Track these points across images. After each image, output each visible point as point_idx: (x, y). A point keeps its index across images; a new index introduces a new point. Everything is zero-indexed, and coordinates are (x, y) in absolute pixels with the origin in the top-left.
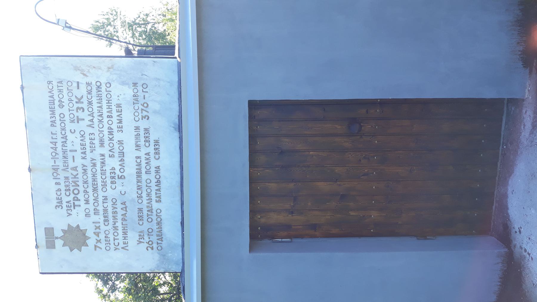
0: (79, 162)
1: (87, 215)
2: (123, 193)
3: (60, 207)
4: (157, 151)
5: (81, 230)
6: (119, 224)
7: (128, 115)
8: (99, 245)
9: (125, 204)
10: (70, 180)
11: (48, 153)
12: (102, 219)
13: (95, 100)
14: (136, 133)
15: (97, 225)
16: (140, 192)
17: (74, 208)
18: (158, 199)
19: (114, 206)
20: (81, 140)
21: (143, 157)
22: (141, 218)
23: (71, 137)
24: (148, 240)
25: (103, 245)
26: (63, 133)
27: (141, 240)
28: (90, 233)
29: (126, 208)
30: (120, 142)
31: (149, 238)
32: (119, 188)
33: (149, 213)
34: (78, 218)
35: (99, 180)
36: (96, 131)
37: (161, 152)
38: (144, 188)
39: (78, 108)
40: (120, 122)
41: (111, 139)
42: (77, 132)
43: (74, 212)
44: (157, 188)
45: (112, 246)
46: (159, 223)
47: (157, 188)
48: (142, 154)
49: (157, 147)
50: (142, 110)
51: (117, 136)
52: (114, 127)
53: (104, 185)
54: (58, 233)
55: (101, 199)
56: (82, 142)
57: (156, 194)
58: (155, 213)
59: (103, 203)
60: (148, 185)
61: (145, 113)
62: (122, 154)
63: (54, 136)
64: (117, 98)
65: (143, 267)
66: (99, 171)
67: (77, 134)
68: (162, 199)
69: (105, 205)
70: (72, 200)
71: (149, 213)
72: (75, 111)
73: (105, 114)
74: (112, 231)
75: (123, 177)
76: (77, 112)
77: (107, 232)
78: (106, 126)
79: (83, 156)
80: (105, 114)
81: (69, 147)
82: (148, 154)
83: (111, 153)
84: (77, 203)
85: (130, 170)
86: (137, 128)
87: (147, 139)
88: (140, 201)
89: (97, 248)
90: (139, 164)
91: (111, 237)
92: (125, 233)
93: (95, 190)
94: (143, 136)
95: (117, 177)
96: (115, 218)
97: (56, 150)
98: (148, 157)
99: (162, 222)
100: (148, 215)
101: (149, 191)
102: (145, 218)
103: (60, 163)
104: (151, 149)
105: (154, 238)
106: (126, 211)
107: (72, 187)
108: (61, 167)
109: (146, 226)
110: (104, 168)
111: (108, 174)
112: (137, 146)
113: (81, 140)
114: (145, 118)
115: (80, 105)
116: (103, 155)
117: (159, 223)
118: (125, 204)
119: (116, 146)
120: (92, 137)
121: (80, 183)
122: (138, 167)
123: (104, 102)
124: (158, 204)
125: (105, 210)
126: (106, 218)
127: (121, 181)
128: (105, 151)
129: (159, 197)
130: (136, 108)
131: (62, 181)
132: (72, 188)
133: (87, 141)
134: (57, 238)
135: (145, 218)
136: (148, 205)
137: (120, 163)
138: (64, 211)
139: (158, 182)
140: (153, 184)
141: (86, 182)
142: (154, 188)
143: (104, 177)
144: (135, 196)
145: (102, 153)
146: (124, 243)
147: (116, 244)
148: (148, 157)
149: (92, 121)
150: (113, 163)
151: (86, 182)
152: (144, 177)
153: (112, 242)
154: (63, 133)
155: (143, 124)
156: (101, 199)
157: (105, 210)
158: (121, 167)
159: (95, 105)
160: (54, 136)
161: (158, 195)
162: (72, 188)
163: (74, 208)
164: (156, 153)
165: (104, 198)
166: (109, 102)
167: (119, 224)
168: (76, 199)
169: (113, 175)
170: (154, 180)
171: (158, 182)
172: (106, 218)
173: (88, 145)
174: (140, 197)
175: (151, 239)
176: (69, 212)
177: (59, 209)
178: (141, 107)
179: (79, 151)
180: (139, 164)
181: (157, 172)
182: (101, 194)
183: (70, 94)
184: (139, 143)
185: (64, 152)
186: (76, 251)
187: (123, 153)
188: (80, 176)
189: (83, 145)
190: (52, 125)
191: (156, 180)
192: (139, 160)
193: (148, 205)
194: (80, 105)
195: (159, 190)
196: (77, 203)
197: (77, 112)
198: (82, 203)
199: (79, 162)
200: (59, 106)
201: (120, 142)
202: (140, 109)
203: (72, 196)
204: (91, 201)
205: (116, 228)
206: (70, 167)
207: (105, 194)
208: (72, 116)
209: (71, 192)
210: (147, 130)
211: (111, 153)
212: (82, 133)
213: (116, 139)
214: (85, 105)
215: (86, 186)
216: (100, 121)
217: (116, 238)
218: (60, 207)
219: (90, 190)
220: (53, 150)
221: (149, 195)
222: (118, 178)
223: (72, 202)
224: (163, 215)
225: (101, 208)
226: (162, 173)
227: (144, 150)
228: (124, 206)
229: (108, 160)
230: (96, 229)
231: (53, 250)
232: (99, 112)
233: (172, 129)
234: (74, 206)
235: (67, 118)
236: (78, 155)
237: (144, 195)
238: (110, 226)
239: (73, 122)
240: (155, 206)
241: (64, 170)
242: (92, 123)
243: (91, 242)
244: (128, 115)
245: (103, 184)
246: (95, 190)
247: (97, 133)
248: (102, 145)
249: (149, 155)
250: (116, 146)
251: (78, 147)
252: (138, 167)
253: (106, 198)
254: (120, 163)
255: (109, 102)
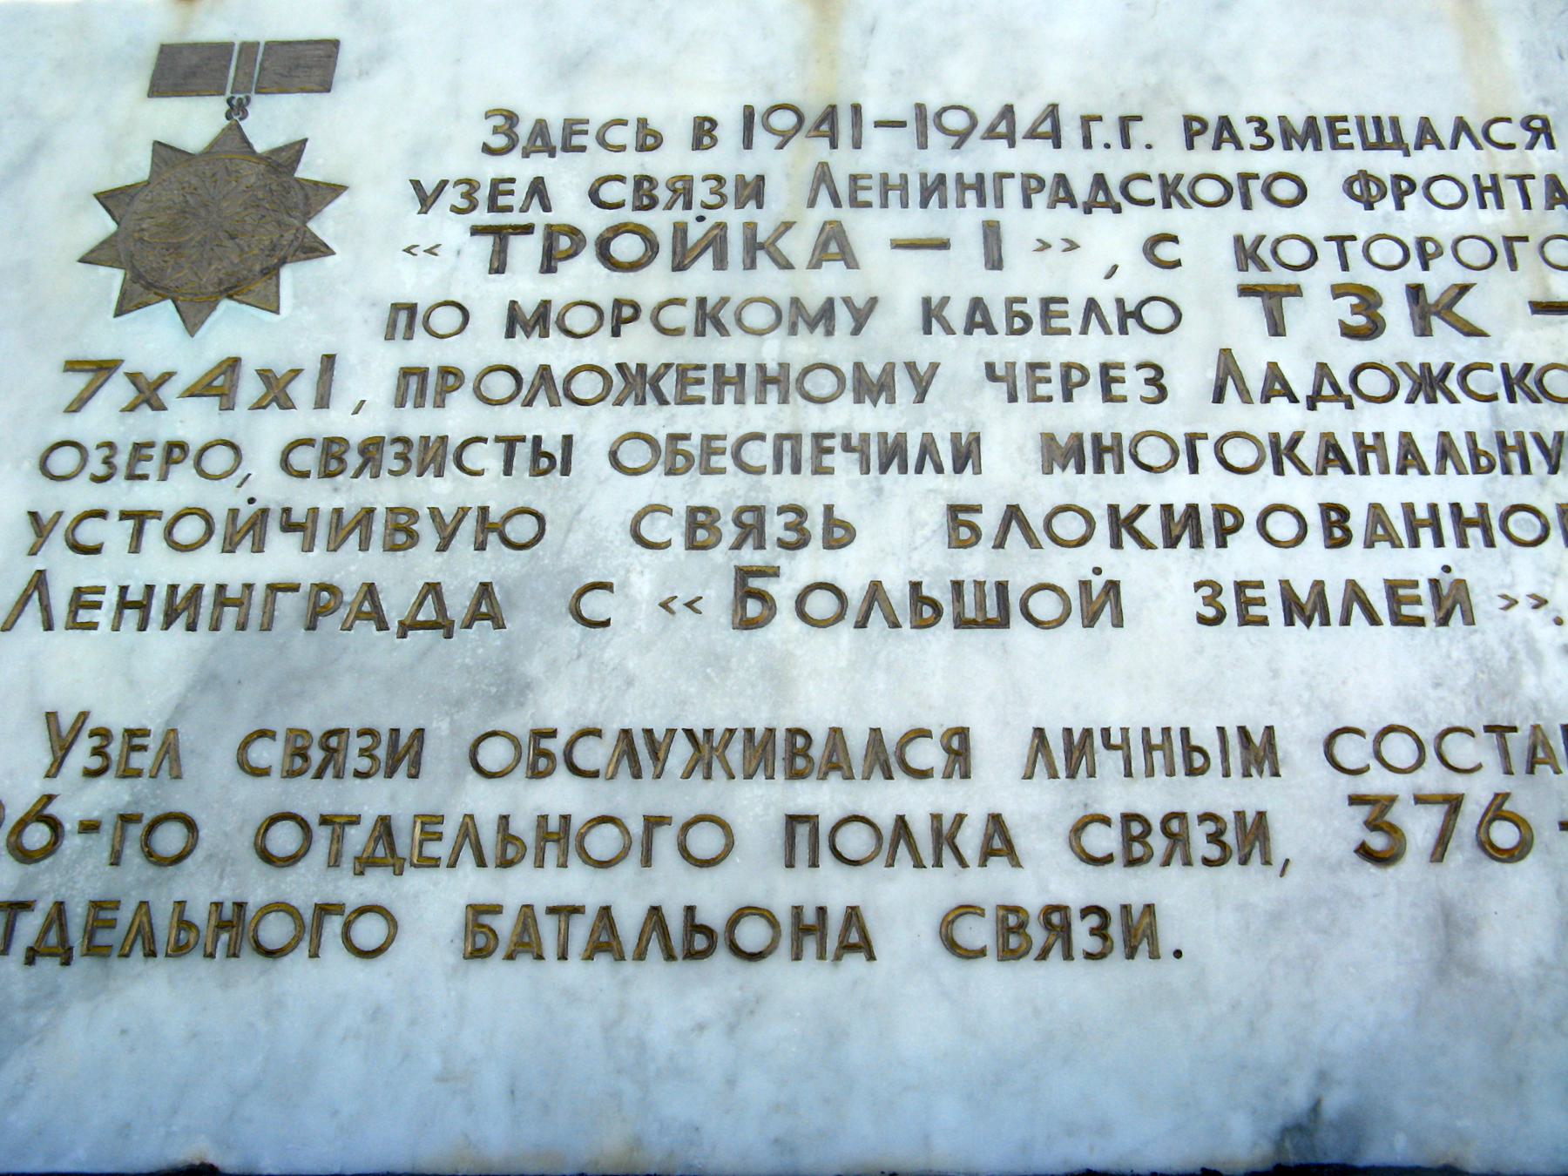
0: (901, 282)
1: (405, 318)
2: (594, 605)
3: (499, 141)
4: (1037, 933)
5: (272, 273)
6: (282, 558)
7: (1377, 673)
8: (118, 390)
9: (474, 617)
10: (734, 218)
11: (966, 82)
12: (356, 429)
13: (1463, 418)
14: (1204, 737)
15: (302, 390)
16: (592, 754)
17: (476, 231)
18: (504, 925)
19: (469, 525)
20: (1092, 306)
21: (969, 801)
22: (316, 753)
23: (1114, 238)
24: (69, 811)
25: (105, 419)
26: (1139, 190)
27: (84, 745)
28: (233, 330)
29: (443, 625)
30: (1102, 602)
31: (89, 827)
32: (643, 577)
33: (357, 838)
34: (379, 256)
35: (727, 419)
36: (1189, 407)
37: (1027, 972)
38: (632, 799)
39: (1368, 301)
40: (1304, 608)
41: (1123, 525)
42: (1160, 282)
43: (448, 228)
44: (629, 923)
45: (79, 496)
46: (235, 930)
47: (629, 923)
48: (999, 786)
49: (1081, 933)
50: (1454, 803)
51: (1161, 581)
52: (1245, 557)
53: (673, 455)
54: (272, 121)
55: (545, 422)
56: (1076, 309)
57: (565, 912)
58: (353, 890)
59: (510, 443)
60: (665, 841)
61: (1420, 827)
62: (991, 610)
63: (1104, 132)
64: (1521, 592)
65: (1107, 146)
66: (813, 419)
67: (1138, 280)
68: (501, 978)
69: (487, 458)
70: (553, 218)
71: (357, 838)
72: (1342, 278)
73: (1356, 493)
74: (220, 499)
75: (753, 608)
76: (1338, 291)
77: (218, 460)
78: (1250, 495)
79: (956, 314)
80: (1356, 493)
81: (1024, 224)
82: (1000, 841)
83: (989, 521)
84: (525, 250)
85: (827, 680)
86: (1259, 752)
87: (1158, 842)
88: (495, 754)
89: (79, 381)
90: (886, 758)
91: (181, 489)
92: (183, 607)
93: (638, 383)
94: (1192, 810)
95: (750, 556)
96: (352, 527)
97: (991, 134)
98: (970, 839)
99: (250, 962)
100: (337, 823)
101: (603, 842)
102: (313, 797)
103: (881, 153)
104: (1047, 878)
105: (79, 875)
106: (405, 629)
107: (675, 214)
108: (844, 162)
109: (224, 799)
110: (839, 460)
111: (780, 489)
112: (1079, 749)
113: (1092, 306)
114: (1373, 825)
115: (1396, 311)
116: (967, 454)
117: (235, 930)
118: (474, 617)
119: (1065, 568)
120: (1134, 384)
121: (701, 279)
122: (857, 743)
123: (1467, 490)
124: (453, 920)
125: (432, 455)
126: (353, 459)
127: (719, 595)
128: (1009, 473)
129: (526, 944)
130: (1461, 750)
131: (726, 158)
132: (660, 221)
133: (1091, 349)
134: (237, 109)
135: (313, 797)
136: (450, 829)
137: (898, 593)
138: (463, 159)
139: (695, 940)
140: (674, 886)
141: (708, 317)
142: (628, 895)
143: (758, 454)
144: (558, 708)
145: (990, 453)
146: (81, 599)
147: (89, 533)
148: (970, 839)
149: (1276, 385)
150: (896, 536)
151: (708, 317)
152: (756, 804)
153: (122, 495)
154: (1139, 190)
155: (1307, 809)
156: (545, 422)
157: (432, 455)
158: (856, 597)
159: (1425, 422)
160: (1104, 132)
161: (548, 928)
162: (660, 221)
163: (476, 231)
164: (1011, 922)
165: (552, 445)
166: (1472, 524)
167: (282, 558)
168: (564, 243)
169: (775, 527)
170: (713, 896)
171: (695, 940)
172: (353, 459)
173: (1058, 351)
174: (540, 755)
175: (73, 842)
176: (452, 196)
177: (483, 132)
178: (1477, 793)
179: (995, 289)
180: (886, 758)
181: (802, 930)
182: (596, 428)
183: (1474, 252)
184: (1110, 762)
185: (980, 188)
186: (101, 225)
187: (1003, 622)
188: (768, 280)
189: (1046, 315)
190: (1193, 128)
191: (714, 914)
192: (927, 754)
193: (450, 829)
194: (1396, 311)
195: (604, 939)
196: (525, 250)
197: (1338, 291)
198: (526, 283)
199: (901, 282)
200: (1364, 177)
201: (1102, 602)
202: (1457, 784)
203: (593, 222)
204: (528, 353)
205: (249, 529)
206: (846, 215)
207: (591, 458)
208: (1297, 253)
209: (627, 215)
210: (1249, 838)
211: (989, 521)
212: (1157, 315)
213: (1130, 566)
214: (1399, 341)
215: (682, 316)
216: (1282, 453)
217: (154, 529)
218: (499, 141)
219: (638, 346)
220: (986, 117)
221: (559, 837)
222: (743, 574)
223: (535, 216)
224: (323, 980)
225: (458, 417)
226: (798, 983)
227: (1037, 809)
228: (458, 606)
229: (922, 497)
230: (265, 375)
231: (145, 84)
232: (1362, 449)
233: (1298, 1096)
234: (501, 235)
235: (1266, 220)
236: (960, 277)
237: (560, 795)
238: (270, 487)
239: (1246, 253)
240: (435, 900)
241: (823, 175)
242: (1255, 385)
243: (153, 340)
244: (1377, 673)
245: (693, 446)
246: (638, 383)
247: (1174, 418)
248: (1064, 453)
249: (987, 853)
250: (1065, 568)
251: (1027, 277)
252: (857, 743)
253: (551, 460)
254: (898, 593)
255: (1472, 524)
